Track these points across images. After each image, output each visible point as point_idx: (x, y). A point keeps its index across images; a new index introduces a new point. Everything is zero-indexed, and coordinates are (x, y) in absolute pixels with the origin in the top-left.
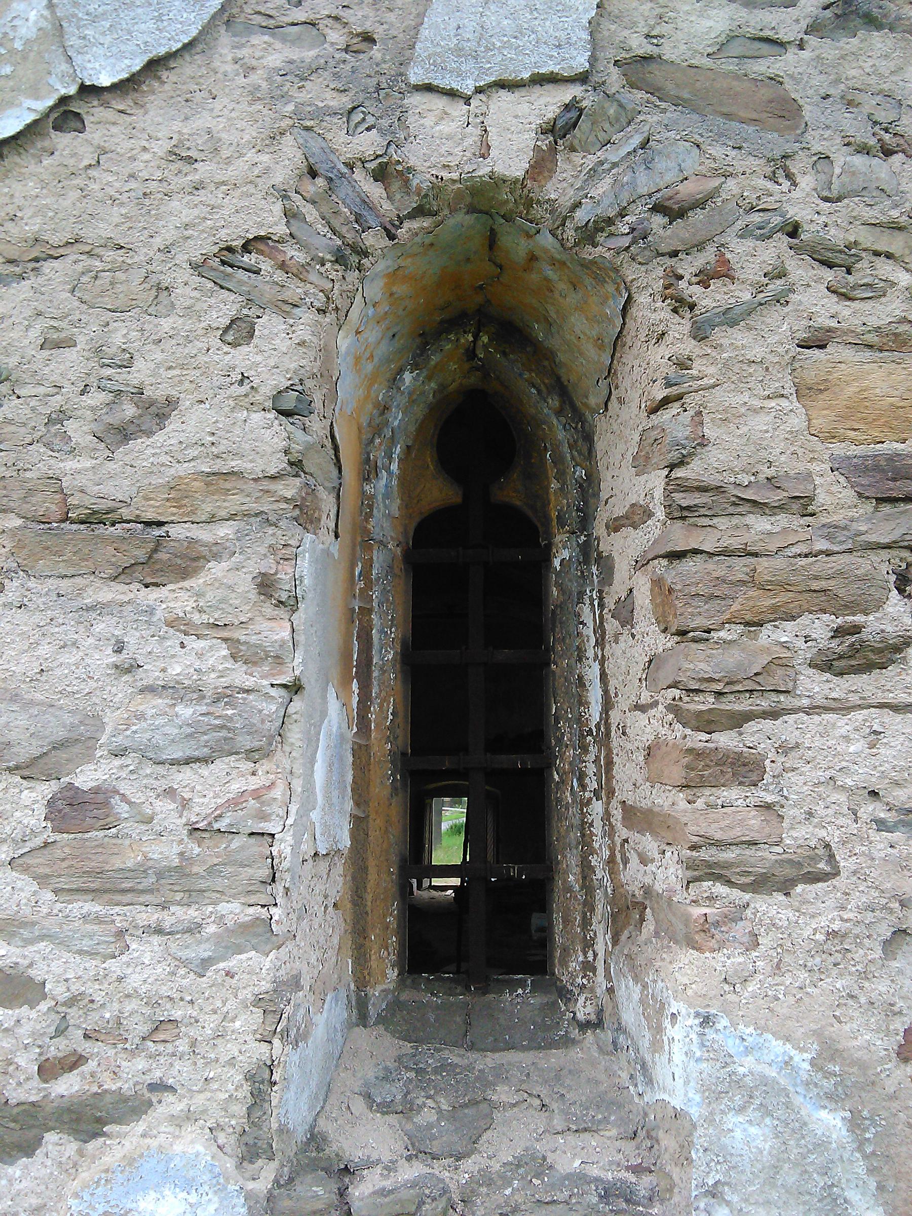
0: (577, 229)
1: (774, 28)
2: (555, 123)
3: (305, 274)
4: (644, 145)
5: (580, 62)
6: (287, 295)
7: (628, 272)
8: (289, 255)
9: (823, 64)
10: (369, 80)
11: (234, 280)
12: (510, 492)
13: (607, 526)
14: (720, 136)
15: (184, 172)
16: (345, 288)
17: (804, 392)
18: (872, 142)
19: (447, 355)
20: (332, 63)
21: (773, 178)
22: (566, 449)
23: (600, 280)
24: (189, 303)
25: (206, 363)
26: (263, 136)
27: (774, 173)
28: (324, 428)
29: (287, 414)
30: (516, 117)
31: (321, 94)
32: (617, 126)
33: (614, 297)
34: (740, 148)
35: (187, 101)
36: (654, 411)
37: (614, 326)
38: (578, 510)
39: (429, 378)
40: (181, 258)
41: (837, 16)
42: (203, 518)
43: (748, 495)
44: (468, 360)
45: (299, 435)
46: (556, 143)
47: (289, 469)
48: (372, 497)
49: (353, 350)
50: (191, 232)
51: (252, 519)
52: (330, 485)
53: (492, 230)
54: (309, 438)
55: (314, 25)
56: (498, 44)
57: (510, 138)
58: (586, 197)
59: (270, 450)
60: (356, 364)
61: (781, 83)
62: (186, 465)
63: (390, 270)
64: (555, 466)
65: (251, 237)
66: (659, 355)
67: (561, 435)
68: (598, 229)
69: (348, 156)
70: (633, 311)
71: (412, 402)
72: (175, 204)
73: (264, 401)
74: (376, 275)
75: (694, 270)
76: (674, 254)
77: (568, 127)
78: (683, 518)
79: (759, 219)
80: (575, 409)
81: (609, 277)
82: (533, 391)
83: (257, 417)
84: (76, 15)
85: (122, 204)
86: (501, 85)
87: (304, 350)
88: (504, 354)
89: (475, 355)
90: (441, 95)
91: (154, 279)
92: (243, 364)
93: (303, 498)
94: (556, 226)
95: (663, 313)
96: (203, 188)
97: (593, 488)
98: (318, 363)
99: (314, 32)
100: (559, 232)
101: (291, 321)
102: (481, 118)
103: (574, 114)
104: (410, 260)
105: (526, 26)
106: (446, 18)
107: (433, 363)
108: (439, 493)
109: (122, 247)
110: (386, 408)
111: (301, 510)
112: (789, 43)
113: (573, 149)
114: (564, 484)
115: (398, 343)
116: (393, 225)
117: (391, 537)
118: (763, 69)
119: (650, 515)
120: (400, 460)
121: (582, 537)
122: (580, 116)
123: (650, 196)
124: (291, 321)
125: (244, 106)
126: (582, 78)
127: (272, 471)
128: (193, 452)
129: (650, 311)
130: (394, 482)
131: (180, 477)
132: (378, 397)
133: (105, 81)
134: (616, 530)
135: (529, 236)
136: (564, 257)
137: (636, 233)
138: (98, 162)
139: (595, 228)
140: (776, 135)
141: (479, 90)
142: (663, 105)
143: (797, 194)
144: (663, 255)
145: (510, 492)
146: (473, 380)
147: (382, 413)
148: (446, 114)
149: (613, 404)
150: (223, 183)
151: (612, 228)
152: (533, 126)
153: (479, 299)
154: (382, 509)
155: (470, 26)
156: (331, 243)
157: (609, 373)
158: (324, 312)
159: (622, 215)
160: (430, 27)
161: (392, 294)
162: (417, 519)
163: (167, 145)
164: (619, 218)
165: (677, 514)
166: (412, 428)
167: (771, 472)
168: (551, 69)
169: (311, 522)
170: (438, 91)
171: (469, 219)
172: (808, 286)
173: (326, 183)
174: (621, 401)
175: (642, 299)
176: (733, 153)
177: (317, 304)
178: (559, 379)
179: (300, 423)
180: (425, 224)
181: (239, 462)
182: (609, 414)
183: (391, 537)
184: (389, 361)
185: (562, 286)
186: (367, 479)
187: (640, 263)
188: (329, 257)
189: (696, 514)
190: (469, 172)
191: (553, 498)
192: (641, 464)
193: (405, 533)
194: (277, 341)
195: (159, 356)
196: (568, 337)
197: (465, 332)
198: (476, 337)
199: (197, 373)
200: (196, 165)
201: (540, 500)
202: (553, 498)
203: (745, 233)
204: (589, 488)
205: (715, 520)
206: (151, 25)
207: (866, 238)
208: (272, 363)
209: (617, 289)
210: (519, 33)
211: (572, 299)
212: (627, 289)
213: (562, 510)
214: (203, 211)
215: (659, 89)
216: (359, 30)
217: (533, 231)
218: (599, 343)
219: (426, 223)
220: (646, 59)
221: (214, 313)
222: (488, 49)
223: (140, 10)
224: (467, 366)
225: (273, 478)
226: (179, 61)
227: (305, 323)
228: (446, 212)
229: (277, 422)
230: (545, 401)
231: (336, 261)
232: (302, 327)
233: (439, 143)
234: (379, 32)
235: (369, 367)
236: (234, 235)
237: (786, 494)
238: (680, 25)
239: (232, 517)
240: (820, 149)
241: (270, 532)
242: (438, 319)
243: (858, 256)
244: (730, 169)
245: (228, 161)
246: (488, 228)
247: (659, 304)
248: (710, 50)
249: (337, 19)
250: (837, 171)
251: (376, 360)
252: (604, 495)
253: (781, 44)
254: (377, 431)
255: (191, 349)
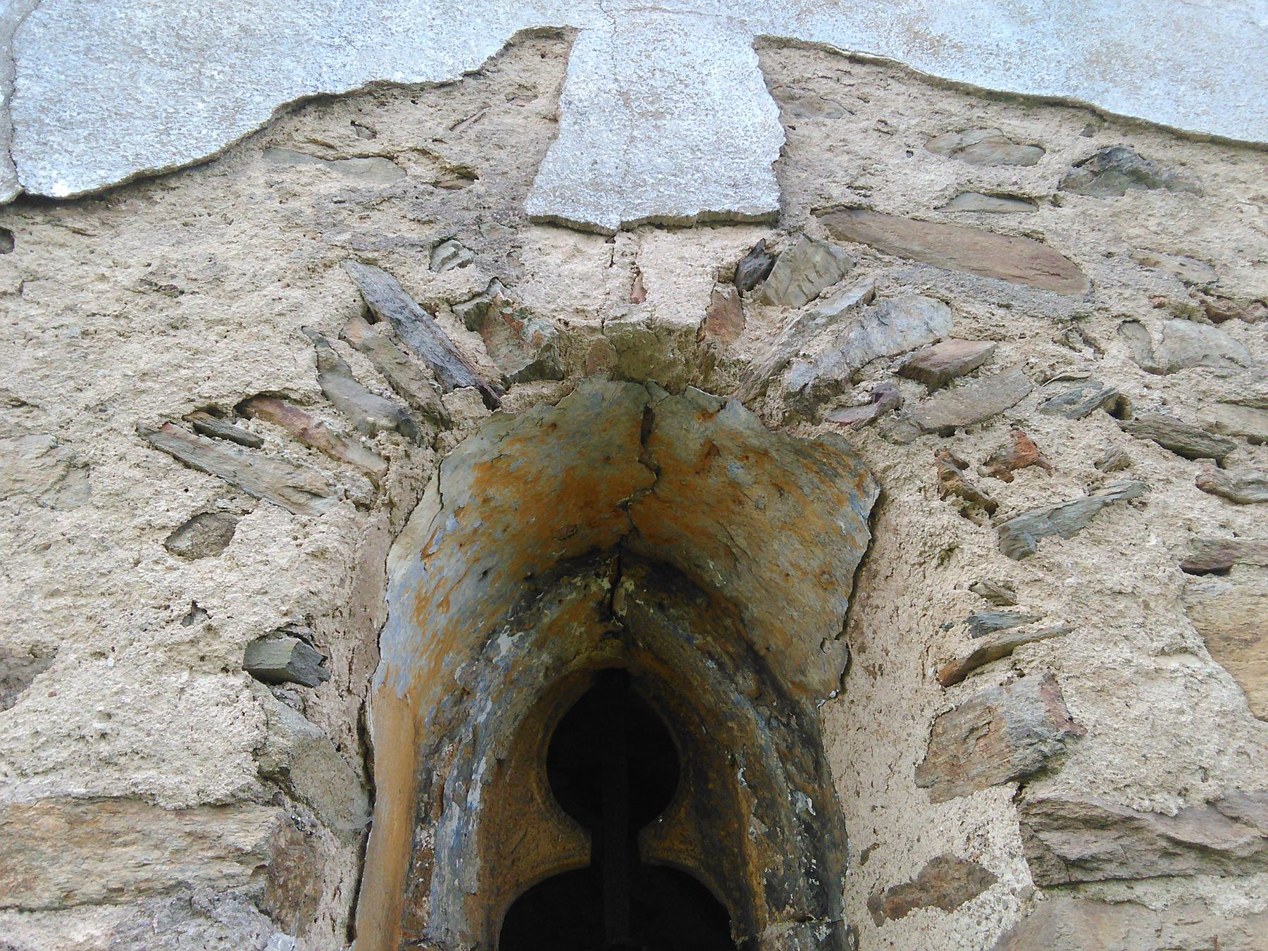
0: (787, 396)
1: (1016, 183)
2: (737, 269)
3: (341, 449)
4: (870, 299)
5: (768, 201)
6: (303, 478)
7: (877, 457)
8: (316, 421)
9: (1092, 221)
10: (466, 213)
11: (212, 454)
12: (675, 842)
13: (874, 906)
14: (977, 293)
15: (159, 307)
16: (407, 471)
17: (1220, 643)
18: (1193, 303)
19: (569, 608)
20: (412, 193)
21: (1065, 342)
22: (774, 760)
23: (828, 474)
24: (119, 485)
25: (127, 584)
26: (295, 266)
27: (1067, 337)
28: (346, 712)
29: (271, 678)
30: (682, 258)
31: (390, 223)
32: (826, 277)
33: (852, 498)
34: (1008, 307)
35: (185, 225)
36: (954, 678)
37: (854, 546)
38: (808, 874)
39: (540, 645)
40: (123, 420)
41: (1095, 174)
42: (46, 898)
43: (1186, 833)
44: (601, 621)
45: (291, 720)
46: (741, 295)
47: (257, 787)
48: (429, 855)
49: (414, 583)
50: (150, 384)
51: (158, 901)
52: (346, 826)
53: (648, 412)
54: (311, 728)
55: (391, 158)
56: (651, 181)
57: (678, 284)
58: (797, 355)
59: (221, 747)
60: (419, 610)
61: (1042, 241)
62: (36, 781)
63: (486, 458)
64: (755, 793)
65: (253, 392)
66: (950, 584)
67: (763, 737)
68: (821, 399)
69: (428, 295)
70: (891, 516)
71: (510, 683)
72: (134, 346)
73: (229, 652)
74: (463, 461)
75: (983, 456)
76: (948, 432)
77: (755, 276)
78: (1073, 885)
79: (1065, 391)
80: (781, 694)
81: (845, 466)
82: (711, 664)
83: (208, 684)
84: (41, 121)
85: (42, 345)
86: (658, 223)
87: (322, 565)
88: (661, 607)
89: (613, 613)
90: (570, 232)
91: (65, 451)
92: (199, 587)
93: (280, 852)
94: (751, 396)
95: (945, 516)
96: (185, 327)
97: (830, 832)
98: (347, 590)
99: (391, 165)
100: (757, 405)
101: (304, 518)
102: (631, 259)
103: (764, 261)
104: (518, 446)
105: (687, 165)
106: (578, 153)
107: (546, 620)
108: (552, 845)
109: (24, 404)
110: (466, 692)
111: (272, 879)
112: (1041, 198)
113: (766, 301)
114: (775, 823)
115: (492, 587)
116: (495, 390)
117: (463, 934)
118: (1014, 224)
119: (986, 879)
120: (486, 786)
121: (823, 929)
122: (772, 265)
123: (892, 358)
124: (304, 518)
125: (274, 231)
126: (771, 220)
127: (219, 791)
128: (55, 754)
129: (920, 512)
130: (473, 827)
131: (17, 807)
132: (452, 672)
133: (61, 190)
134: (898, 912)
135: (706, 415)
136: (766, 442)
137: (883, 400)
138: (21, 291)
139: (815, 396)
140: (1053, 294)
141: (626, 228)
142: (887, 258)
143: (1107, 362)
144: (930, 431)
145: (675, 842)
146: (610, 651)
147: (459, 701)
148: (579, 251)
149: (858, 679)
150: (220, 322)
151: (843, 398)
152: (709, 269)
153: (621, 526)
154: (448, 876)
155: (610, 162)
156: (389, 403)
157: (845, 625)
158: (368, 508)
159: (854, 380)
160: (555, 161)
161: (486, 501)
162: (510, 898)
163: (138, 272)
164: (850, 385)
165: (1058, 876)
166: (508, 730)
167: (1211, 789)
168: (727, 207)
169: (295, 906)
170: (567, 228)
171: (614, 389)
172: (1168, 482)
173: (390, 327)
174: (874, 672)
175: (906, 497)
176: (1002, 312)
177: (356, 494)
178: (750, 647)
179: (296, 697)
180: (545, 391)
181: (153, 772)
182: (847, 698)
183: (463, 934)
184: (475, 615)
185: (757, 492)
186: (424, 820)
187: (896, 443)
188: (384, 422)
189: (1099, 875)
190: (615, 318)
191: (754, 854)
192: (943, 775)
193: (489, 923)
194: (273, 549)
195: (37, 572)
196: (767, 575)
197: (598, 575)
198: (615, 583)
199: (107, 602)
200: (182, 298)
201: (727, 853)
202: (752, 851)
203: (1048, 407)
204: (824, 829)
205: (1139, 890)
206: (151, 137)
207: (1233, 419)
208: (256, 584)
209: (859, 486)
210: (680, 171)
211: (778, 510)
212: (878, 482)
213: (774, 875)
214: (179, 355)
215: (877, 241)
216: (455, 163)
217: (716, 405)
218: (825, 580)
219: (548, 389)
220: (852, 209)
221: (163, 503)
222: (636, 186)
223: (137, 122)
224: (599, 630)
225: (221, 806)
226: (185, 181)
227: (330, 523)
228: (579, 374)
229: (247, 693)
230: (732, 681)
231: (397, 429)
232: (321, 528)
233: (567, 286)
234: (482, 167)
235: (441, 621)
236: (225, 391)
237: (1256, 832)
238: (891, 177)
239: (111, 896)
240: (1124, 310)
241: (192, 931)
242: (556, 555)
243: (1229, 442)
244: (1003, 331)
245: (235, 295)
246: (642, 408)
247: (936, 503)
248: (936, 203)
249: (424, 152)
250: (1157, 336)
251: (454, 609)
252: (856, 844)
253: (1029, 200)
254: (448, 731)
255: (102, 561)
